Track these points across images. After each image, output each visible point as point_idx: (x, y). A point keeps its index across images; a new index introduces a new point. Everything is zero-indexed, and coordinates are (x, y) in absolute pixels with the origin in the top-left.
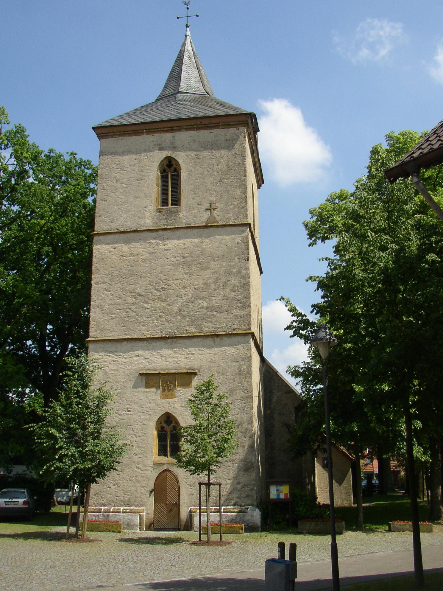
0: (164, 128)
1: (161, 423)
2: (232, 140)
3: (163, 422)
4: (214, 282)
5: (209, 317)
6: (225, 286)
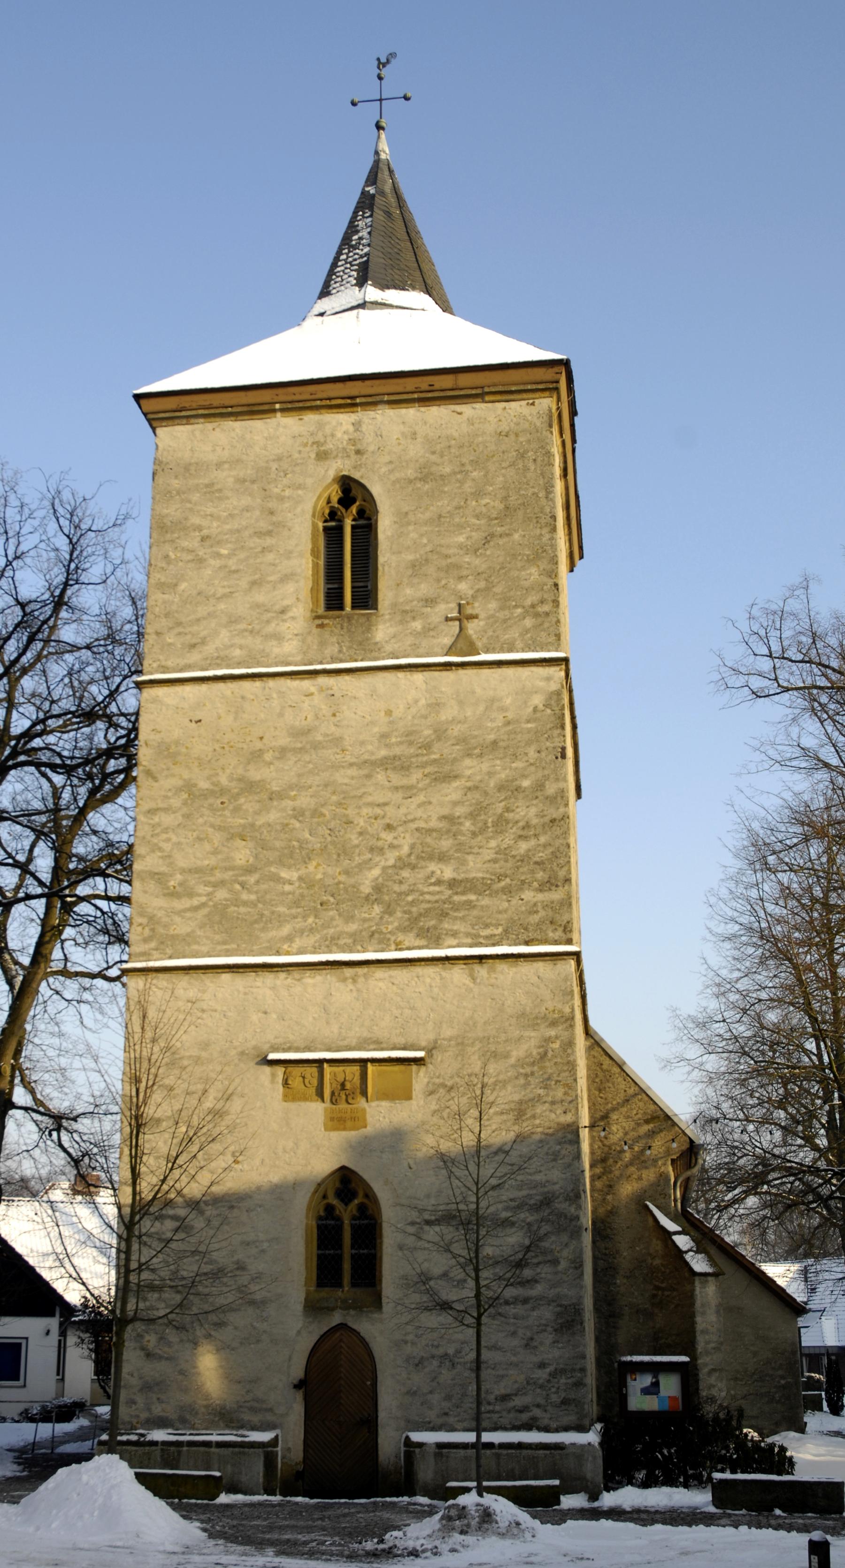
0: (330, 399)
1: (325, 1197)
2: (517, 435)
3: (331, 1194)
4: (472, 816)
5: (456, 907)
6: (501, 824)
